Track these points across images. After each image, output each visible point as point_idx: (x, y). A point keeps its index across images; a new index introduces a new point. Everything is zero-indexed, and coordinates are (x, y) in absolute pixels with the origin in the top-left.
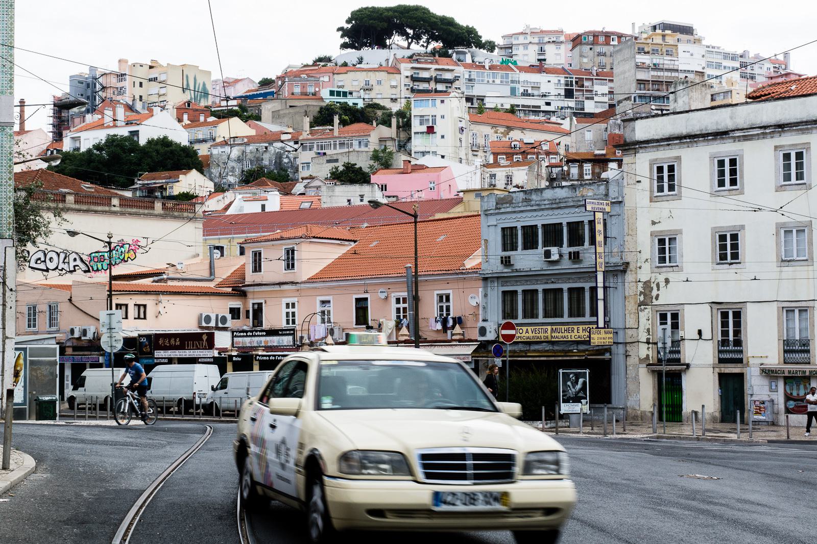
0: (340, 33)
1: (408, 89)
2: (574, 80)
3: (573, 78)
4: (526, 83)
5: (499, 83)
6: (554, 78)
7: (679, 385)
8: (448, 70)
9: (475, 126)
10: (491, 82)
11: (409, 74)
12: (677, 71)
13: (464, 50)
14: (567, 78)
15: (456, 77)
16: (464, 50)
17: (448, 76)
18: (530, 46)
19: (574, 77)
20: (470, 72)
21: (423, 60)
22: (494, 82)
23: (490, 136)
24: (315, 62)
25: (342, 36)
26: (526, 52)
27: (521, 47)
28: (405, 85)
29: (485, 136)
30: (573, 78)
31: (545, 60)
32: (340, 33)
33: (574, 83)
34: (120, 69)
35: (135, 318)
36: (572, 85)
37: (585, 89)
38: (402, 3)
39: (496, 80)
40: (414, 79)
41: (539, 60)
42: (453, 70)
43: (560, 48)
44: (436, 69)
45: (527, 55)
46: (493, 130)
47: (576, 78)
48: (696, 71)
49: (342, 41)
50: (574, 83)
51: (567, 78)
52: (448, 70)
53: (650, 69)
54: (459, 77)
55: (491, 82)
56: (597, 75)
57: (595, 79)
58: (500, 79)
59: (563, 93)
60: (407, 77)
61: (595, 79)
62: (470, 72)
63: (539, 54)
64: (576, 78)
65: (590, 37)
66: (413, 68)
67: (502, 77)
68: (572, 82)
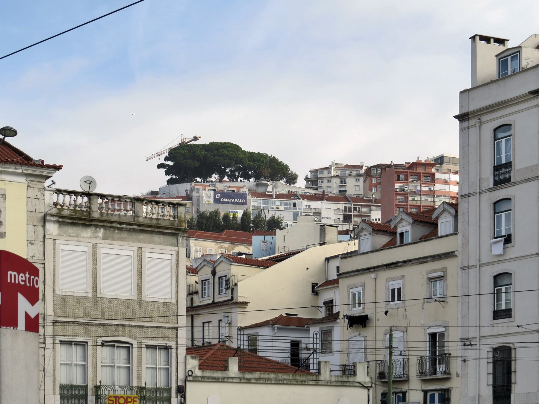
0: (163, 170)
2: (353, 206)
4: (307, 210)
5: (283, 209)
6: (333, 206)
7: (245, 154)
12: (27, 175)
13: (267, 182)
16: (267, 182)
26: (329, 184)
27: (325, 181)
31: (345, 191)
32: (163, 170)
34: (518, 171)
35: (508, 40)
36: (351, 211)
41: (340, 191)
43: (359, 180)
45: (330, 187)
47: (354, 205)
49: (168, 177)
57: (372, 206)
59: (342, 217)
61: (372, 206)
63: (341, 186)
68: (350, 208)
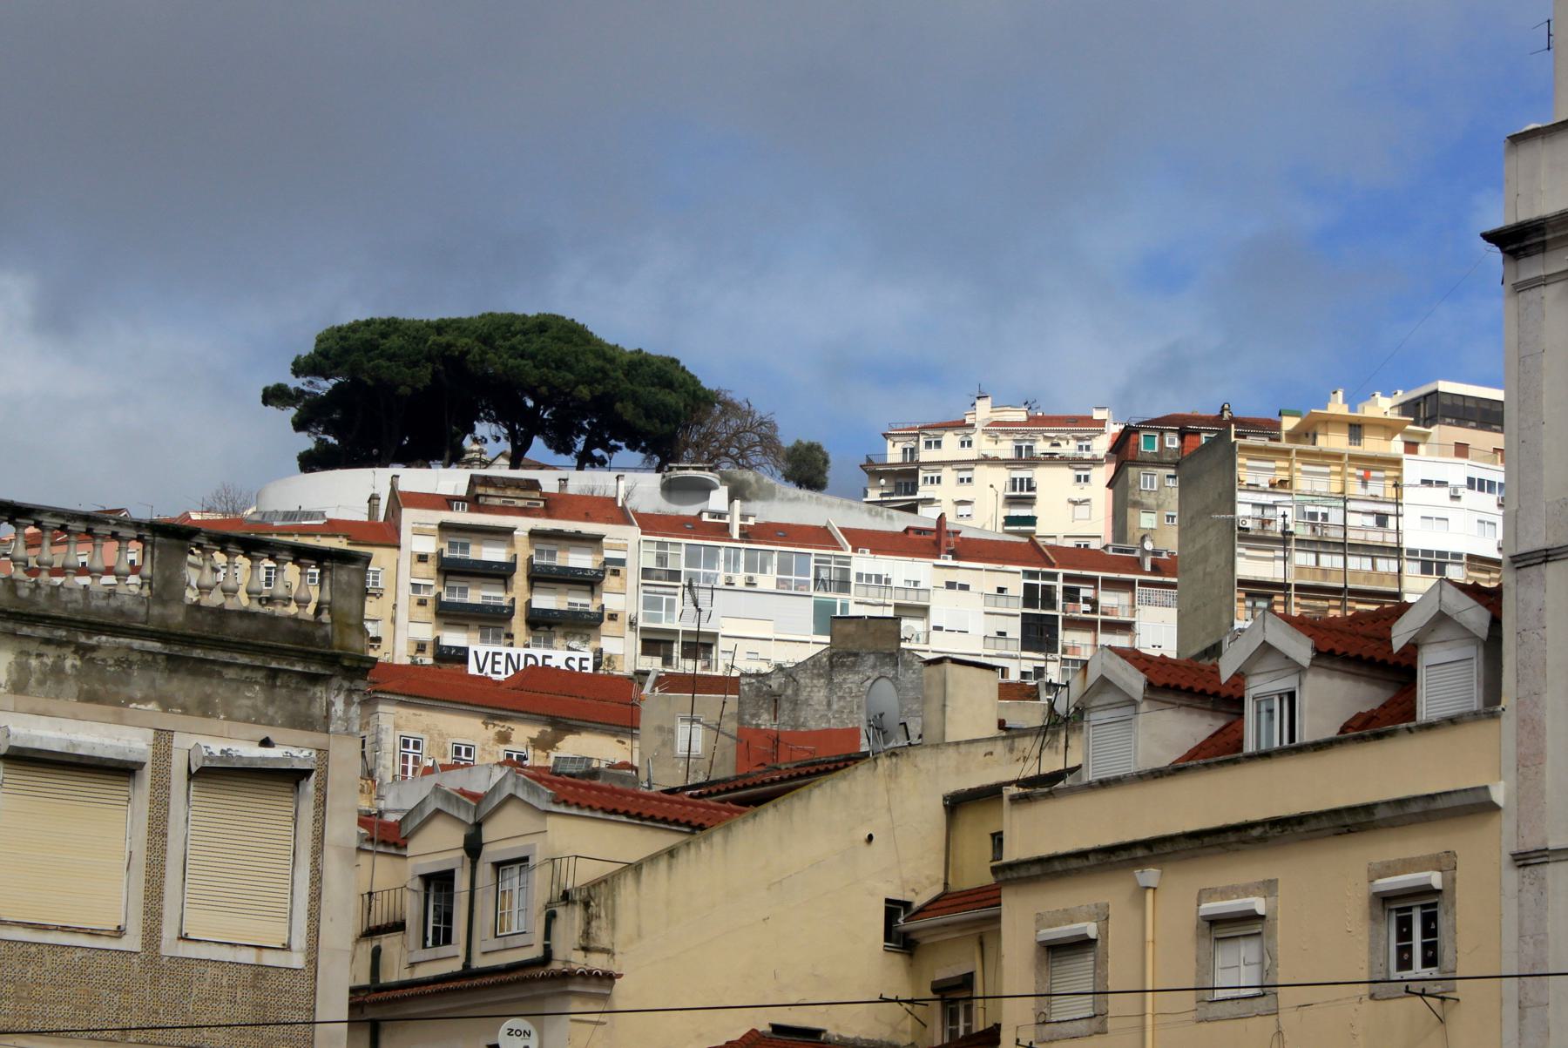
1: (422, 603)
2: (1059, 585)
3: (1054, 576)
5: (773, 588)
6: (982, 577)
8: (578, 539)
9: (412, 711)
10: (740, 582)
11: (429, 545)
14: (1033, 575)
15: (607, 561)
17: (580, 560)
18: (981, 472)
19: (1061, 572)
20: (662, 545)
21: (497, 502)
22: (750, 582)
23: (477, 752)
24: (1342, 731)
25: (300, 425)
26: (964, 492)
28: (416, 587)
29: (458, 751)
30: (1054, 576)
33: (1059, 596)
36: (1049, 601)
37: (1099, 617)
38: (542, 312)
39: (759, 578)
40: (450, 570)
41: (1010, 521)
42: (597, 539)
43: (1087, 478)
44: (534, 534)
46: (492, 731)
47: (1067, 578)
48: (1471, 557)
49: (306, 442)
50: (1059, 596)
51: (1033, 575)
52: (578, 539)
53: (1293, 546)
54: (622, 562)
55: (740, 582)
56: (1156, 569)
57: (1142, 583)
58: (776, 575)
59: (1014, 629)
60: (422, 558)
61: (1142, 583)
62: (662, 545)
64: (1067, 578)
65: (1167, 437)
66: (444, 527)
67: (784, 568)
68: (1049, 591)
